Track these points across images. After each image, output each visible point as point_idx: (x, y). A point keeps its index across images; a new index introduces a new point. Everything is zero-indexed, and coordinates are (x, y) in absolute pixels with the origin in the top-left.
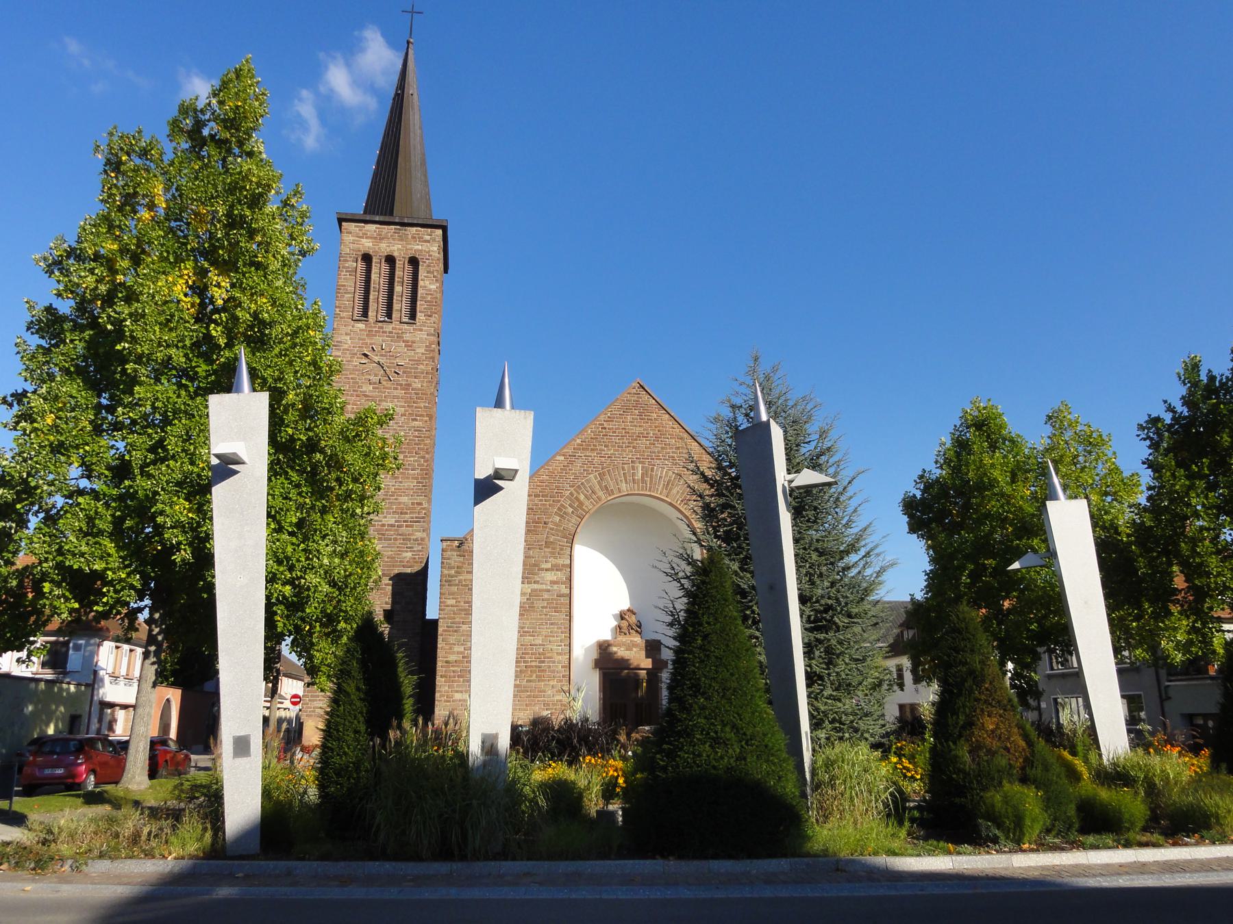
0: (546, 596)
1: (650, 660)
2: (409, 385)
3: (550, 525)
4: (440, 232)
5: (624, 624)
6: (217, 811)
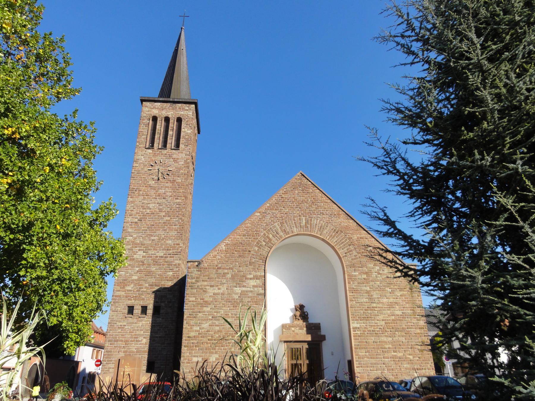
0: (250, 294)
1: (310, 335)
3: (252, 252)
5: (298, 313)
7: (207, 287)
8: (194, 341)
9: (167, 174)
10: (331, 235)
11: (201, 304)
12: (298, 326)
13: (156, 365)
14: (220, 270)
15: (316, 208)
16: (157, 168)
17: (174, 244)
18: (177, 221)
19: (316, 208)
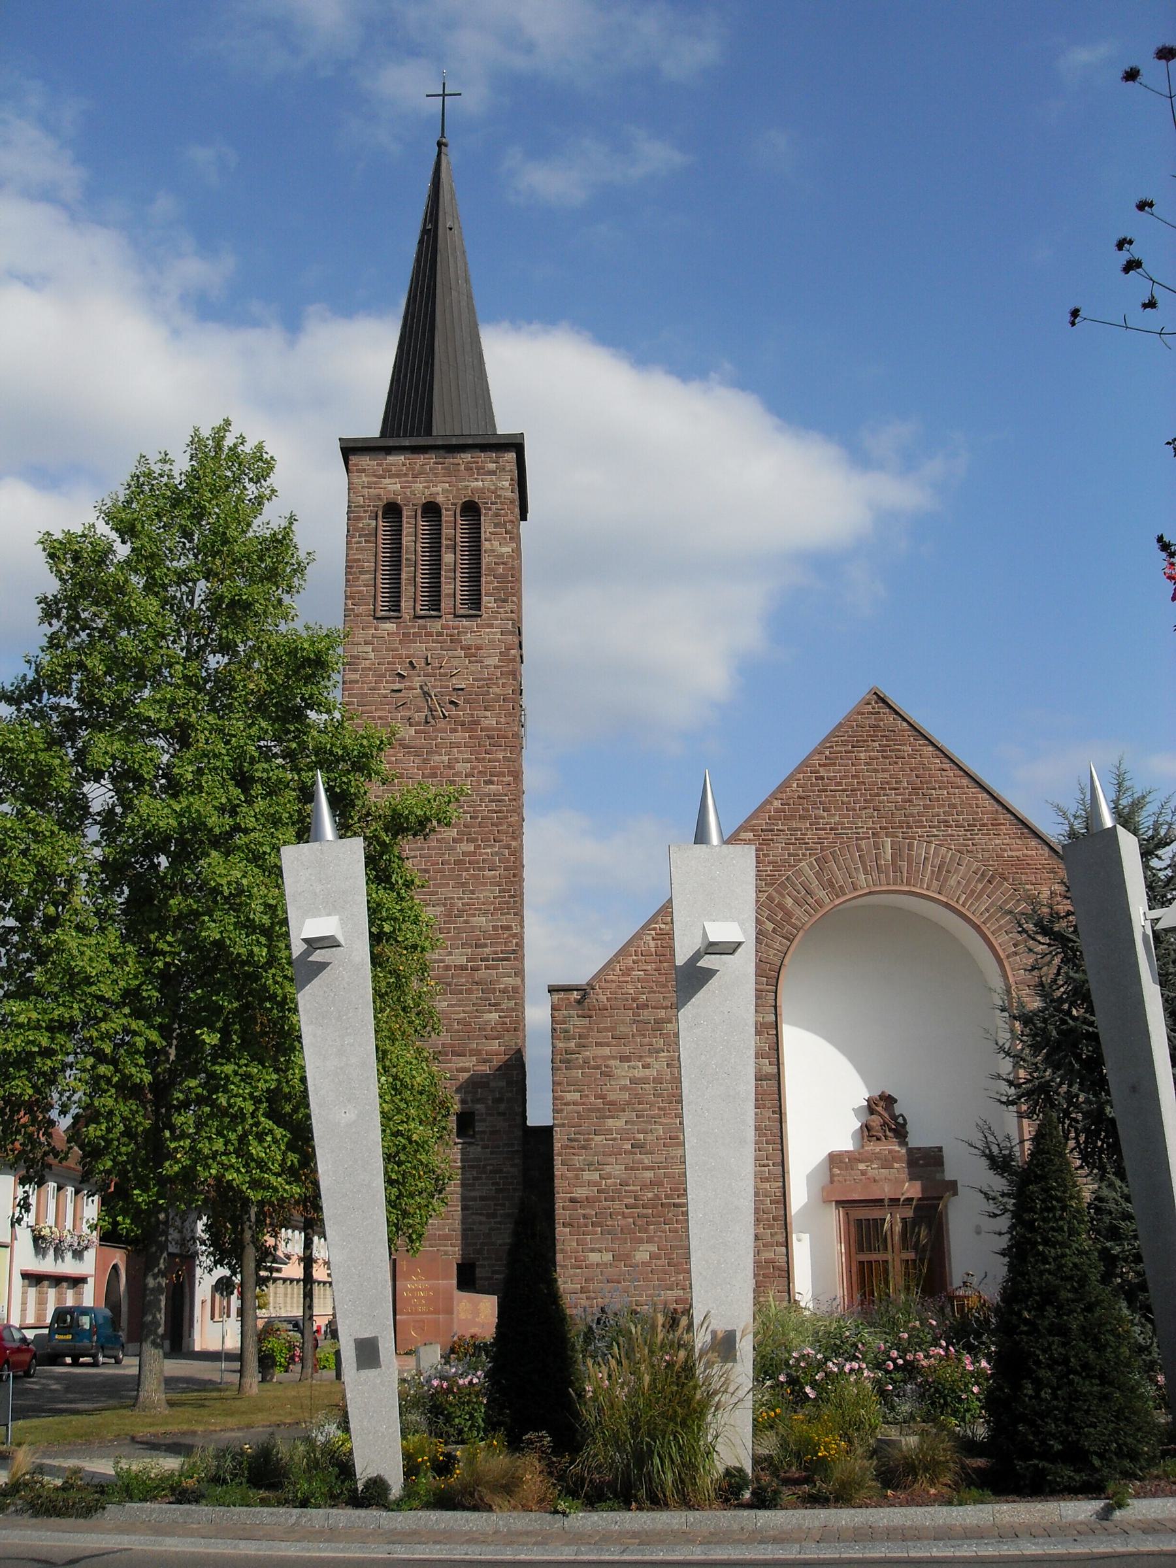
1: (918, 1185)
2: (477, 723)
4: (512, 456)
5: (876, 1121)
6: (827, 1500)
7: (612, 1063)
8: (588, 1211)
9: (452, 702)
10: (973, 892)
11: (598, 1110)
12: (876, 1157)
13: (479, 1272)
14: (646, 1012)
15: (926, 807)
16: (417, 681)
17: (495, 928)
18: (497, 854)
19: (926, 807)
